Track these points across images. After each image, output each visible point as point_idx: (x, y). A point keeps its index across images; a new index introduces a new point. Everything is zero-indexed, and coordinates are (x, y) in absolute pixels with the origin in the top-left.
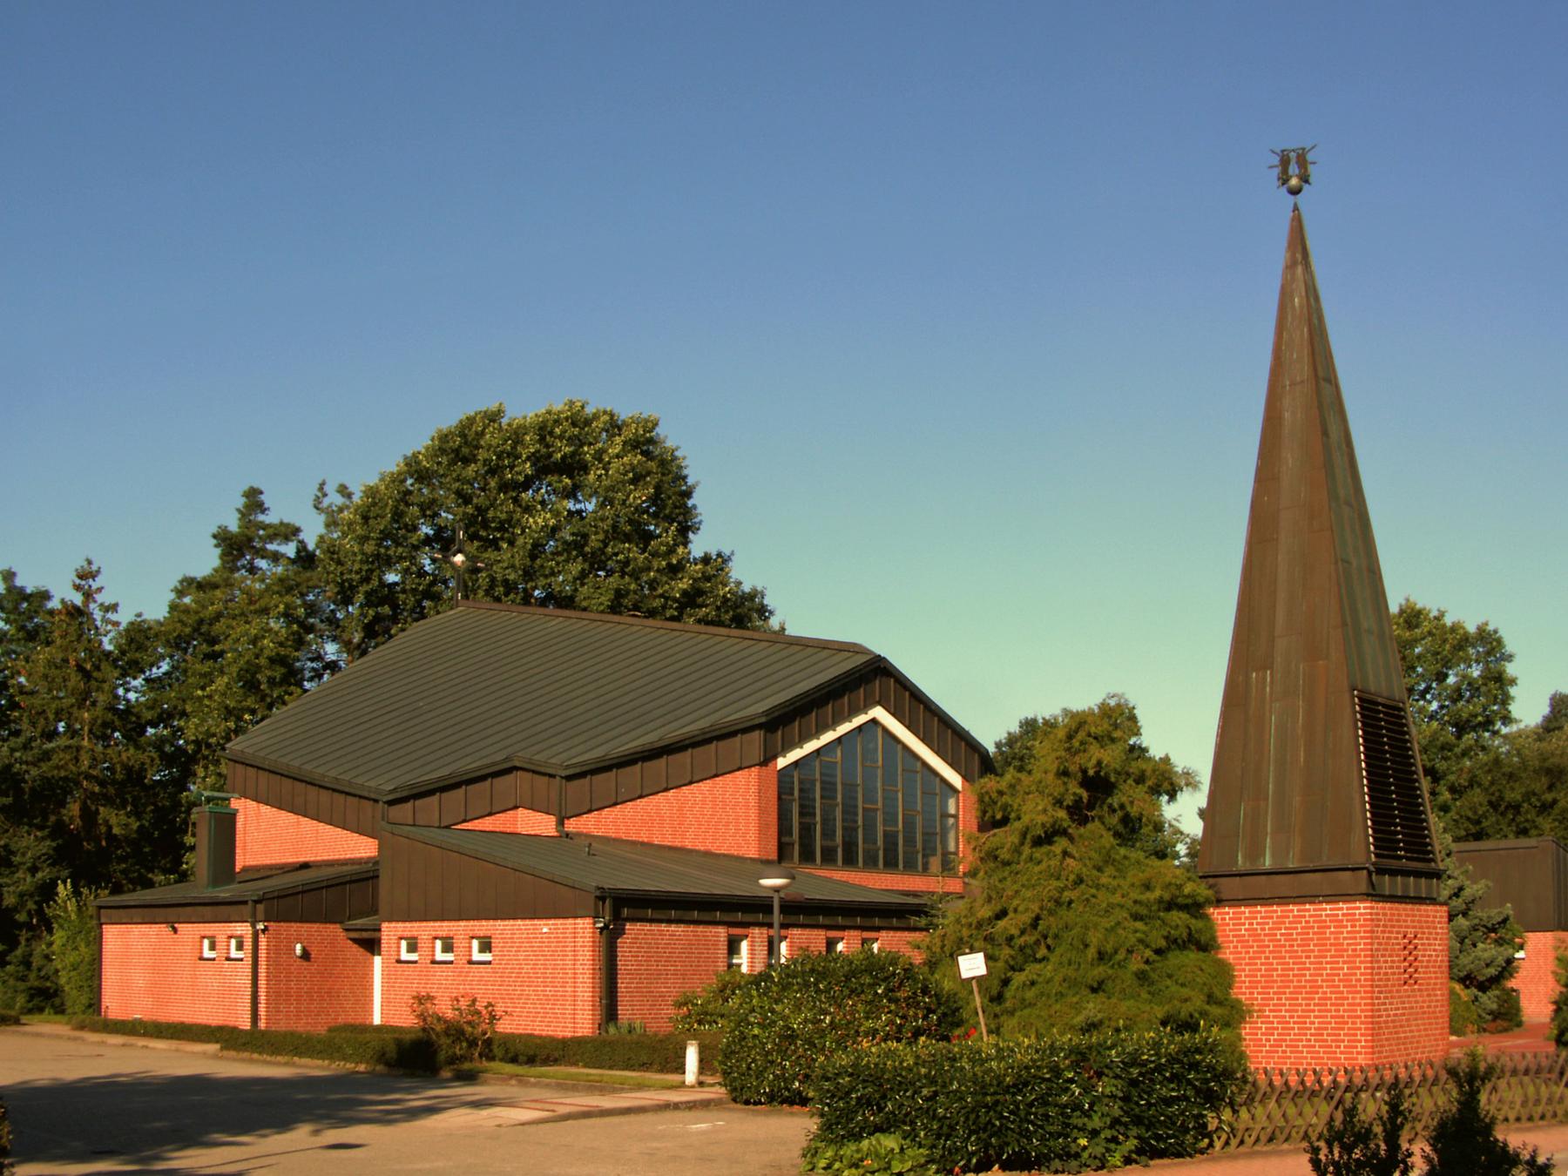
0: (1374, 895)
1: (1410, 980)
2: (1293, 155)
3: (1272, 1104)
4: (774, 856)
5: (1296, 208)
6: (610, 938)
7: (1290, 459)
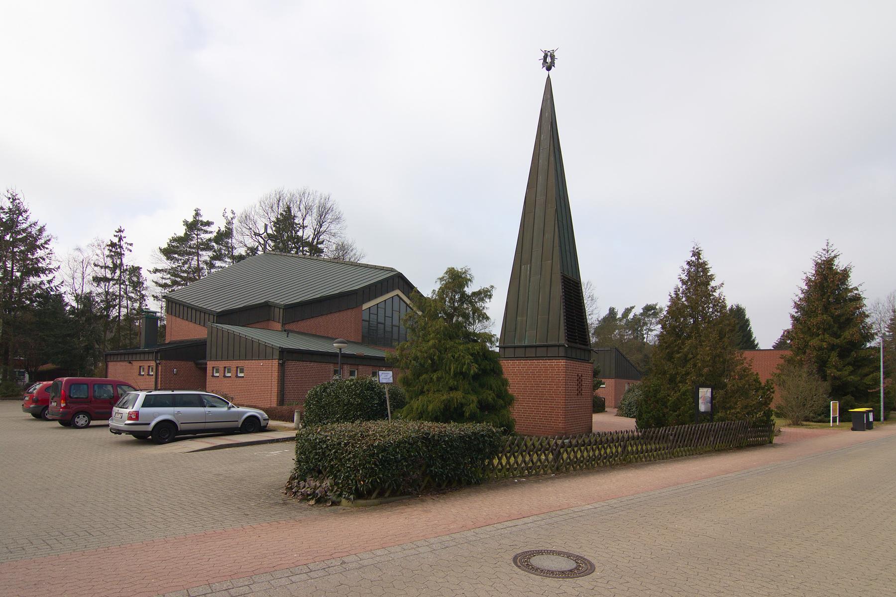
0: (566, 357)
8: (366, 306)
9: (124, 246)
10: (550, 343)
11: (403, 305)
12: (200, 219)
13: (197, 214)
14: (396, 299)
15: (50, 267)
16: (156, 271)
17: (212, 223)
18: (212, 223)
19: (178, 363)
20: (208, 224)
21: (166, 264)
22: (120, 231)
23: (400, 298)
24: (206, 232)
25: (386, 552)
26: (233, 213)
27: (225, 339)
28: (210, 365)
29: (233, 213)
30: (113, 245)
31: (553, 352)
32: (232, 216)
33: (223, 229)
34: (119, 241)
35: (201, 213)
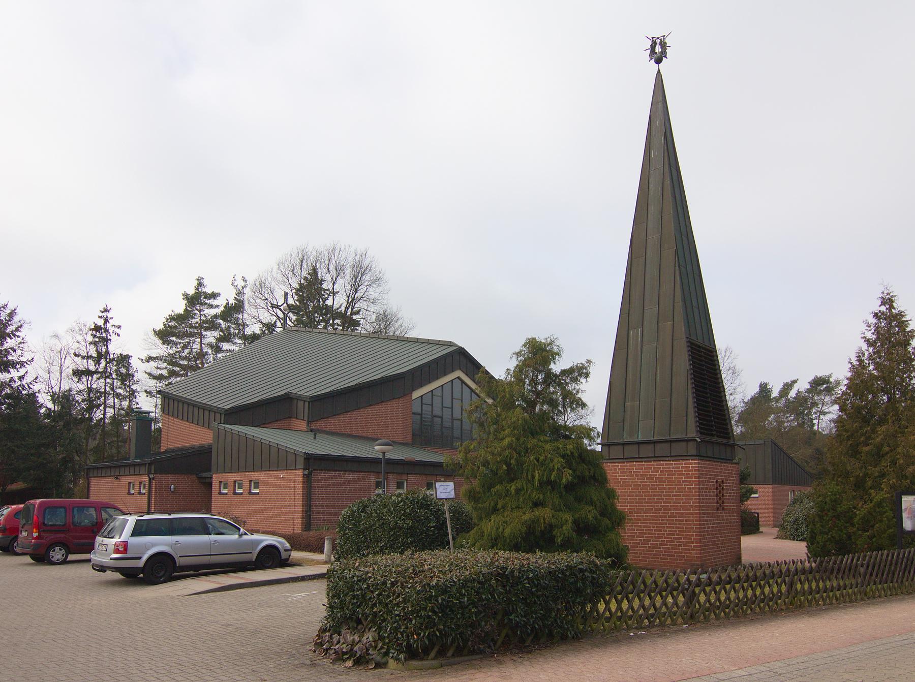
0: (699, 456)
1: (720, 506)
2: (658, 41)
3: (734, 576)
4: (410, 442)
5: (659, 75)
6: (307, 478)
7: (653, 210)
8: (416, 394)
9: (111, 329)
12: (204, 290)
13: (200, 284)
15: (22, 359)
17: (218, 295)
18: (218, 295)
20: (214, 296)
21: (161, 350)
22: (106, 310)
23: (463, 382)
24: (211, 306)
26: (244, 280)
28: (216, 478)
29: (244, 280)
30: (97, 328)
31: (678, 449)
32: (243, 284)
33: (232, 301)
34: (105, 323)
35: (205, 282)
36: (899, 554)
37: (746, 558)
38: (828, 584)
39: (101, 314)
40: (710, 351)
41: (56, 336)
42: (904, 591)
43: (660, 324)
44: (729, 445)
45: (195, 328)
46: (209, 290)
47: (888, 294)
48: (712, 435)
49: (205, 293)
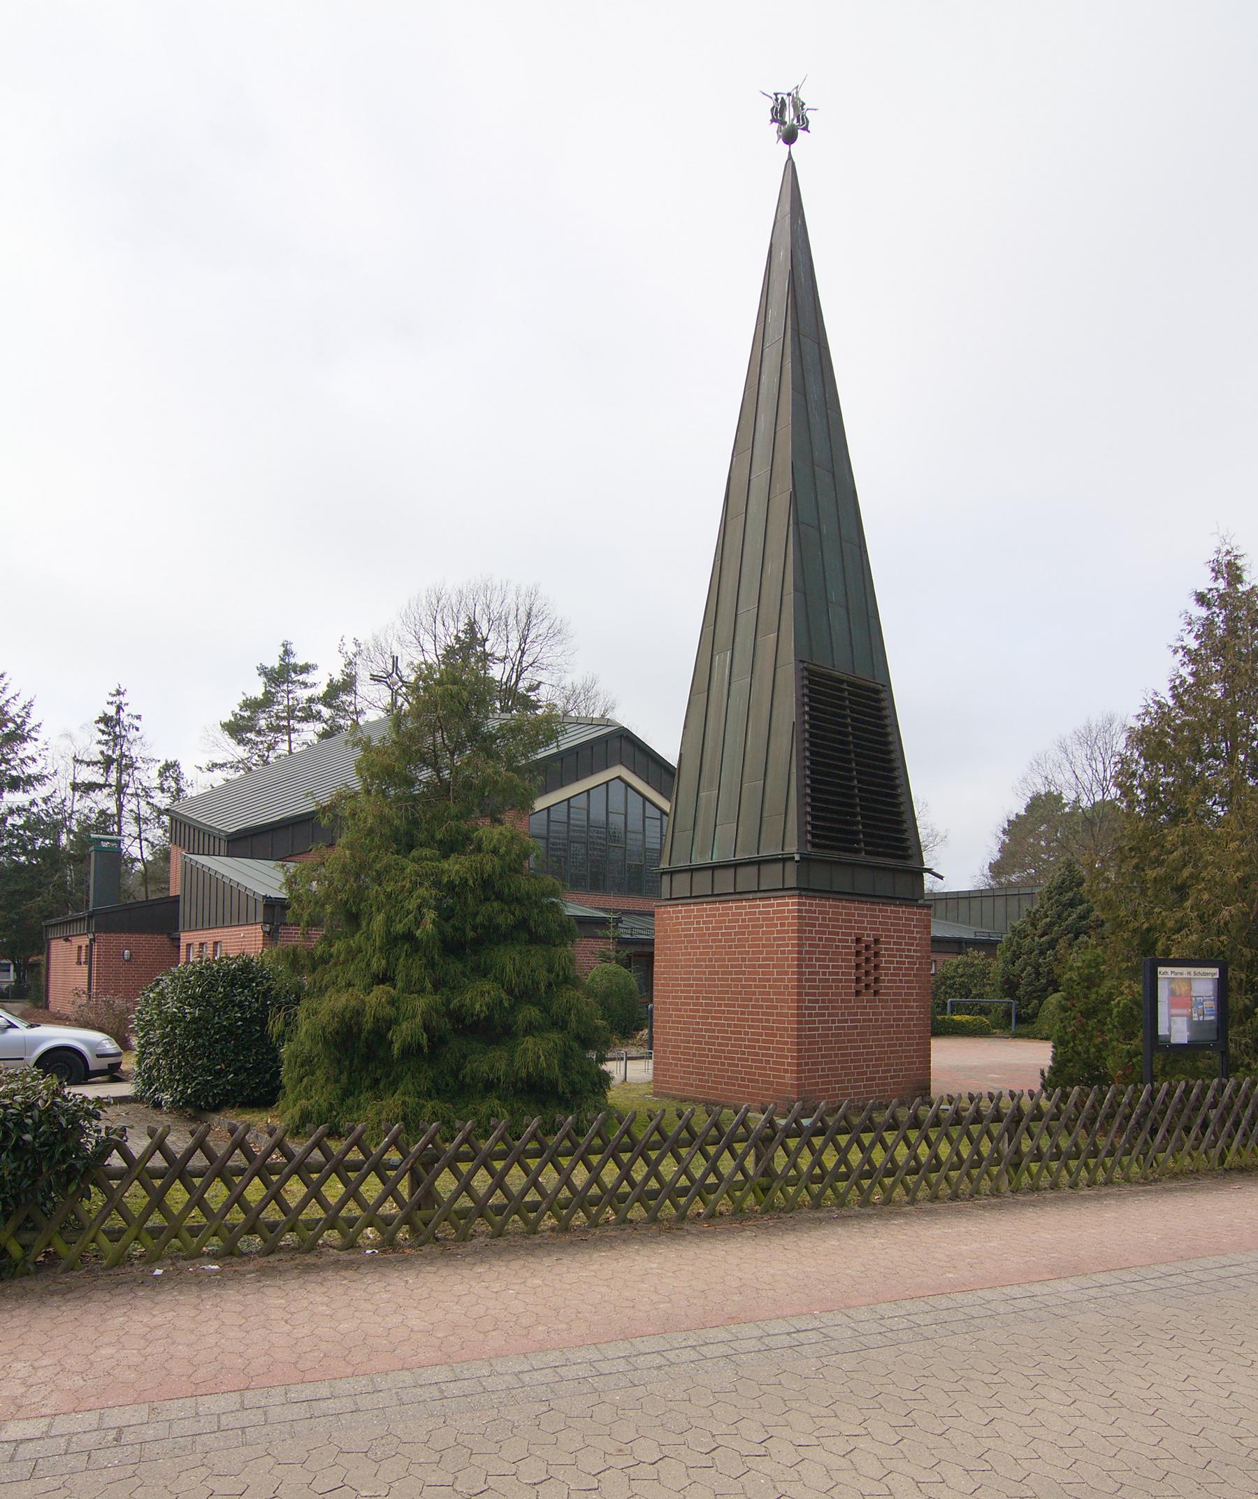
0: (804, 890)
5: (790, 158)
8: (541, 804)
9: (126, 720)
10: (764, 853)
11: (635, 803)
12: (292, 661)
13: (287, 652)
14: (617, 787)
15: (45, 773)
16: (214, 766)
17: (315, 667)
18: (315, 667)
19: (134, 938)
20: (306, 669)
21: (234, 751)
22: (119, 693)
23: (628, 785)
24: (305, 685)
25: (766, 1340)
26: (357, 644)
27: (207, 880)
28: (185, 938)
29: (357, 644)
30: (105, 720)
31: (772, 875)
32: (355, 650)
33: (338, 677)
34: (118, 712)
35: (293, 648)
36: (1188, 1090)
37: (940, 1085)
38: (549, 1177)
39: (111, 699)
40: (877, 692)
41: (68, 736)
42: (944, 1189)
43: (759, 637)
44: (911, 872)
45: (283, 718)
46: (299, 660)
47: (1228, 553)
48: (857, 851)
49: (295, 665)
